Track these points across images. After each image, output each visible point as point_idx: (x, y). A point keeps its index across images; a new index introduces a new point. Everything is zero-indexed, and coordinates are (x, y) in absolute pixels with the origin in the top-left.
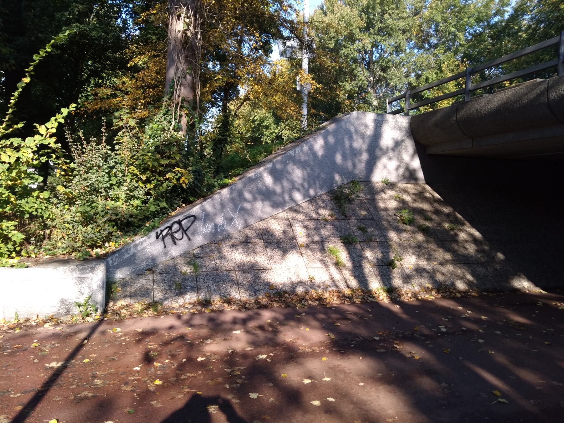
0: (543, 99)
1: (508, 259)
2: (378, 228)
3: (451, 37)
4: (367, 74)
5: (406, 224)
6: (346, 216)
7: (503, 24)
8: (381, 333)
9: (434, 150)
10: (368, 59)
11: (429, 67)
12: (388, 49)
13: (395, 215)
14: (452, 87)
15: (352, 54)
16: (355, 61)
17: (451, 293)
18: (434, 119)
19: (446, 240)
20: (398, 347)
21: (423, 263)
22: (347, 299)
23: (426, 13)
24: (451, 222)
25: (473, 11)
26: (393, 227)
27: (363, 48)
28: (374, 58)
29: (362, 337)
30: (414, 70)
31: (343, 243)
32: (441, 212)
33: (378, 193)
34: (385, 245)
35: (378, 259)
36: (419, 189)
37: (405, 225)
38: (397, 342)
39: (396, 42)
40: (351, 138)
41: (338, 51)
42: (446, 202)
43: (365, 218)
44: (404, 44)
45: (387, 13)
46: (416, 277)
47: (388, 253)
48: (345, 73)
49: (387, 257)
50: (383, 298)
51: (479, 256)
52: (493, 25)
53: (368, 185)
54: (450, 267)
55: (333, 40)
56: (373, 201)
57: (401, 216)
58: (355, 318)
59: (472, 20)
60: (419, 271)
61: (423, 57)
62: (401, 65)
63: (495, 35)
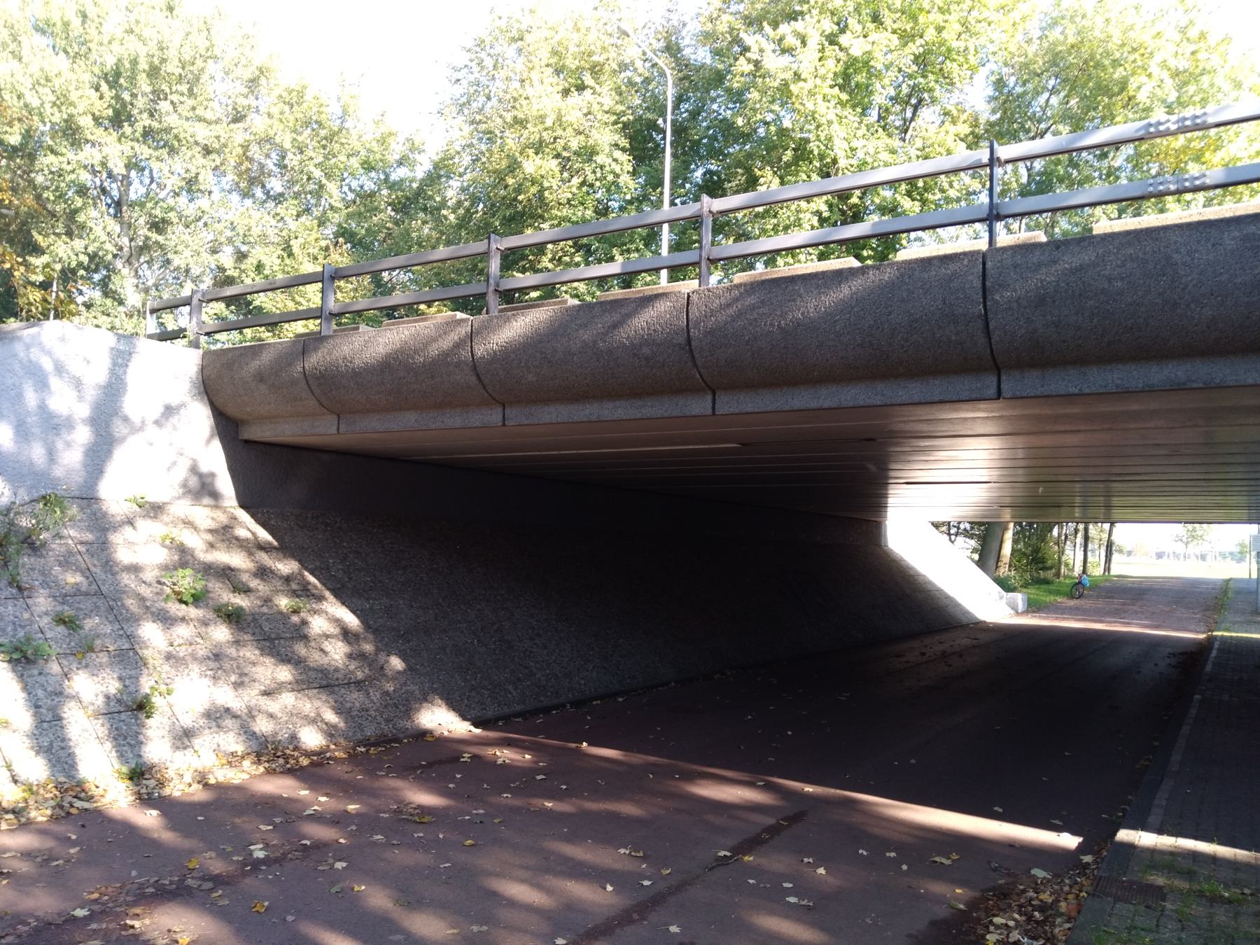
0: (465, 354)
1: (410, 668)
2: (111, 618)
3: (313, 186)
4: (115, 227)
5: (186, 603)
6: (20, 588)
7: (415, 185)
8: (96, 895)
9: (257, 432)
10: (115, 193)
11: (263, 240)
12: (169, 183)
13: (159, 582)
14: (312, 295)
15: (73, 171)
16: (82, 191)
17: (286, 758)
18: (255, 364)
19: (278, 637)
20: (137, 924)
21: (225, 696)
22: (10, 816)
23: (258, 123)
24: (294, 594)
25: (357, 146)
26: (153, 614)
27: (103, 164)
28: (133, 196)
29: (37, 919)
30: (230, 241)
31: (9, 661)
32: (272, 572)
33: (115, 527)
34: (129, 659)
35: (107, 697)
36: (223, 518)
37: (183, 606)
38: (137, 910)
39: (187, 171)
40: (42, 384)
41: (32, 157)
42: (285, 549)
43: (77, 592)
44: (207, 179)
45: (166, 99)
46: (207, 731)
47: (136, 678)
48: (53, 214)
49: (132, 688)
50: (116, 798)
51: (352, 667)
52: (395, 183)
53: (89, 506)
54: (288, 699)
55: (17, 125)
56: (101, 548)
57: (174, 584)
58: (24, 867)
59: (355, 162)
60: (216, 716)
61: (250, 217)
62: (200, 224)
63: (399, 203)
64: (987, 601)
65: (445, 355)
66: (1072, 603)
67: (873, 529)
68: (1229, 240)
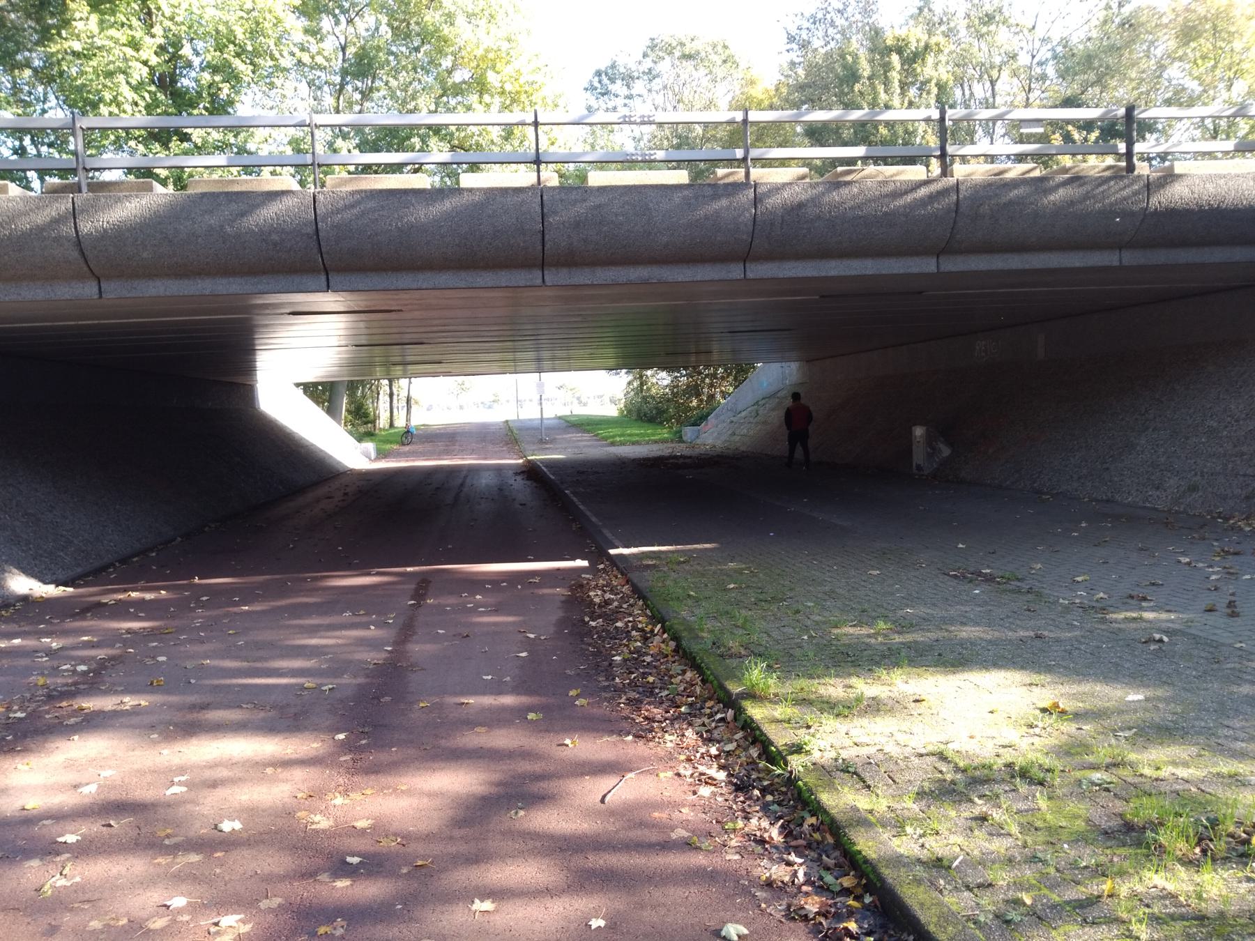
0: (67, 230)
64: (349, 452)
65: (39, 231)
66: (407, 448)
67: (248, 392)
68: (677, 197)
